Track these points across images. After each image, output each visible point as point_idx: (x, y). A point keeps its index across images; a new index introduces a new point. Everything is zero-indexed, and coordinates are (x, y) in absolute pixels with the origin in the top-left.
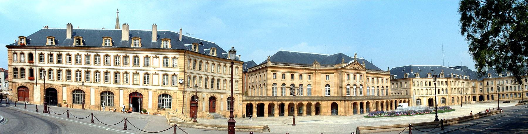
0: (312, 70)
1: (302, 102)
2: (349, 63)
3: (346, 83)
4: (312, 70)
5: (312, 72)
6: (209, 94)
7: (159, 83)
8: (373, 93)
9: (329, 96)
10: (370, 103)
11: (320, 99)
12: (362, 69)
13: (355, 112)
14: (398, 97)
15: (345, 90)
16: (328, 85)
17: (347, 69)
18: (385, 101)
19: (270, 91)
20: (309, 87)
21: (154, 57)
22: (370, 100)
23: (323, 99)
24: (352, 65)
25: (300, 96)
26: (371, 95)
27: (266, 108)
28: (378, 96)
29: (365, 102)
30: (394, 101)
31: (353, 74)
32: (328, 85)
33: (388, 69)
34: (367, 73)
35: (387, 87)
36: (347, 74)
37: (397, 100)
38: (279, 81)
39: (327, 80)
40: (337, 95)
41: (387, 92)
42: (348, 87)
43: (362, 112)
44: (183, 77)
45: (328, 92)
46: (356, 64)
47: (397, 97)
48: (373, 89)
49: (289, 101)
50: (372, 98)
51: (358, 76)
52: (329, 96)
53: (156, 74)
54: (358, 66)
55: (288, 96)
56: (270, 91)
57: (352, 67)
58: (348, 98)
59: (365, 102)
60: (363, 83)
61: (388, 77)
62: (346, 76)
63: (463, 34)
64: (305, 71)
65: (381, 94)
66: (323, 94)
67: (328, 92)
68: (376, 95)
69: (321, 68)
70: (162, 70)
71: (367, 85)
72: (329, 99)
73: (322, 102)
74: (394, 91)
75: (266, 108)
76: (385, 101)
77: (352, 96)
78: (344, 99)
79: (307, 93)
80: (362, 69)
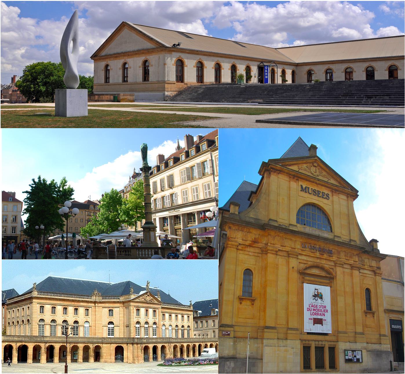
0: (91, 302)
1: (77, 344)
2: (140, 295)
3: (136, 320)
4: (91, 302)
5: (90, 305)
8: (170, 334)
9: (113, 337)
10: (166, 347)
11: (101, 341)
12: (156, 302)
13: (146, 359)
14: (203, 340)
15: (133, 330)
16: (111, 323)
17: (137, 302)
18: (185, 345)
19: (36, 330)
20: (87, 325)
23: (104, 341)
24: (144, 297)
26: (167, 336)
27: (30, 352)
28: (177, 338)
29: (159, 346)
30: (197, 345)
31: (144, 309)
32: (111, 323)
33: (190, 303)
34: (162, 308)
35: (189, 326)
37: (201, 343)
38: (48, 316)
39: (110, 315)
41: (188, 333)
42: (138, 326)
43: (155, 358)
45: (111, 332)
46: (148, 295)
47: (201, 340)
48: (170, 328)
49: (60, 343)
50: (169, 341)
51: (151, 311)
52: (113, 337)
54: (152, 298)
56: (36, 330)
57: (143, 300)
58: (137, 340)
59: (159, 346)
60: (157, 321)
64: (82, 304)
65: (180, 336)
66: (105, 335)
67: (111, 332)
68: (174, 336)
69: (103, 300)
71: (162, 323)
72: (113, 341)
73: (104, 345)
74: (198, 332)
75: (30, 352)
76: (185, 345)
77: (143, 338)
78: (132, 342)
79: (84, 333)
80: (156, 302)
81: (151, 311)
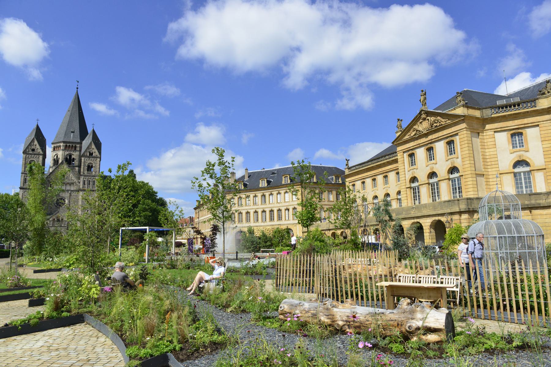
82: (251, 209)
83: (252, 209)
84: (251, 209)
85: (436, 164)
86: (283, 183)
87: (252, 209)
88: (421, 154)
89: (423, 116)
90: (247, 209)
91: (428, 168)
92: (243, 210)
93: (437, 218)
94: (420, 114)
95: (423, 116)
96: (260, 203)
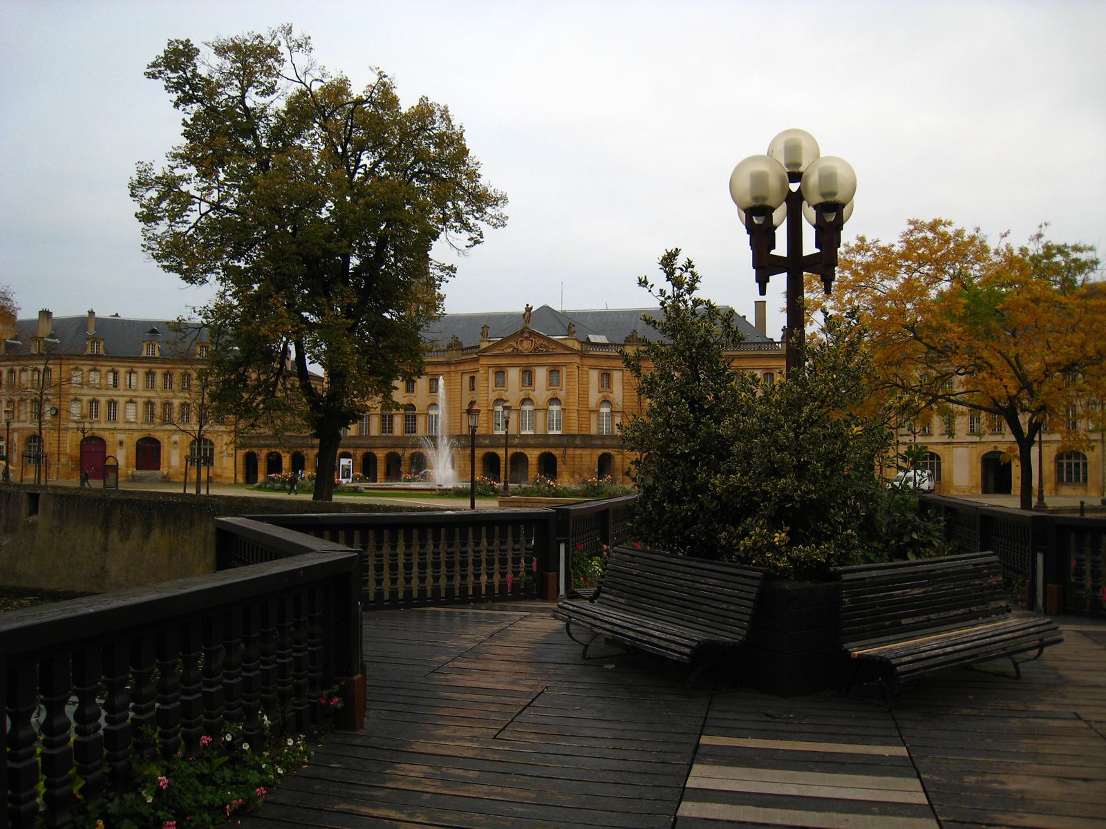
1: (372, 450)
6: (1051, 445)
7: (136, 418)
21: (127, 402)
22: (555, 447)
25: (408, 435)
31: (518, 369)
36: (766, 372)
40: (577, 432)
44: (58, 403)
46: (527, 338)
51: (541, 374)
53: (131, 401)
55: (373, 434)
57: (510, 350)
61: (773, 363)
62: (492, 377)
63: (149, 67)
70: (143, 394)
81: (541, 374)
82: (120, 396)
83: (124, 396)
84: (120, 396)
85: (534, 390)
86: (144, 354)
87: (124, 396)
88: (514, 375)
89: (526, 335)
90: (110, 396)
91: (601, 395)
92: (103, 396)
93: (547, 450)
94: (522, 332)
95: (526, 335)
96: (141, 386)
